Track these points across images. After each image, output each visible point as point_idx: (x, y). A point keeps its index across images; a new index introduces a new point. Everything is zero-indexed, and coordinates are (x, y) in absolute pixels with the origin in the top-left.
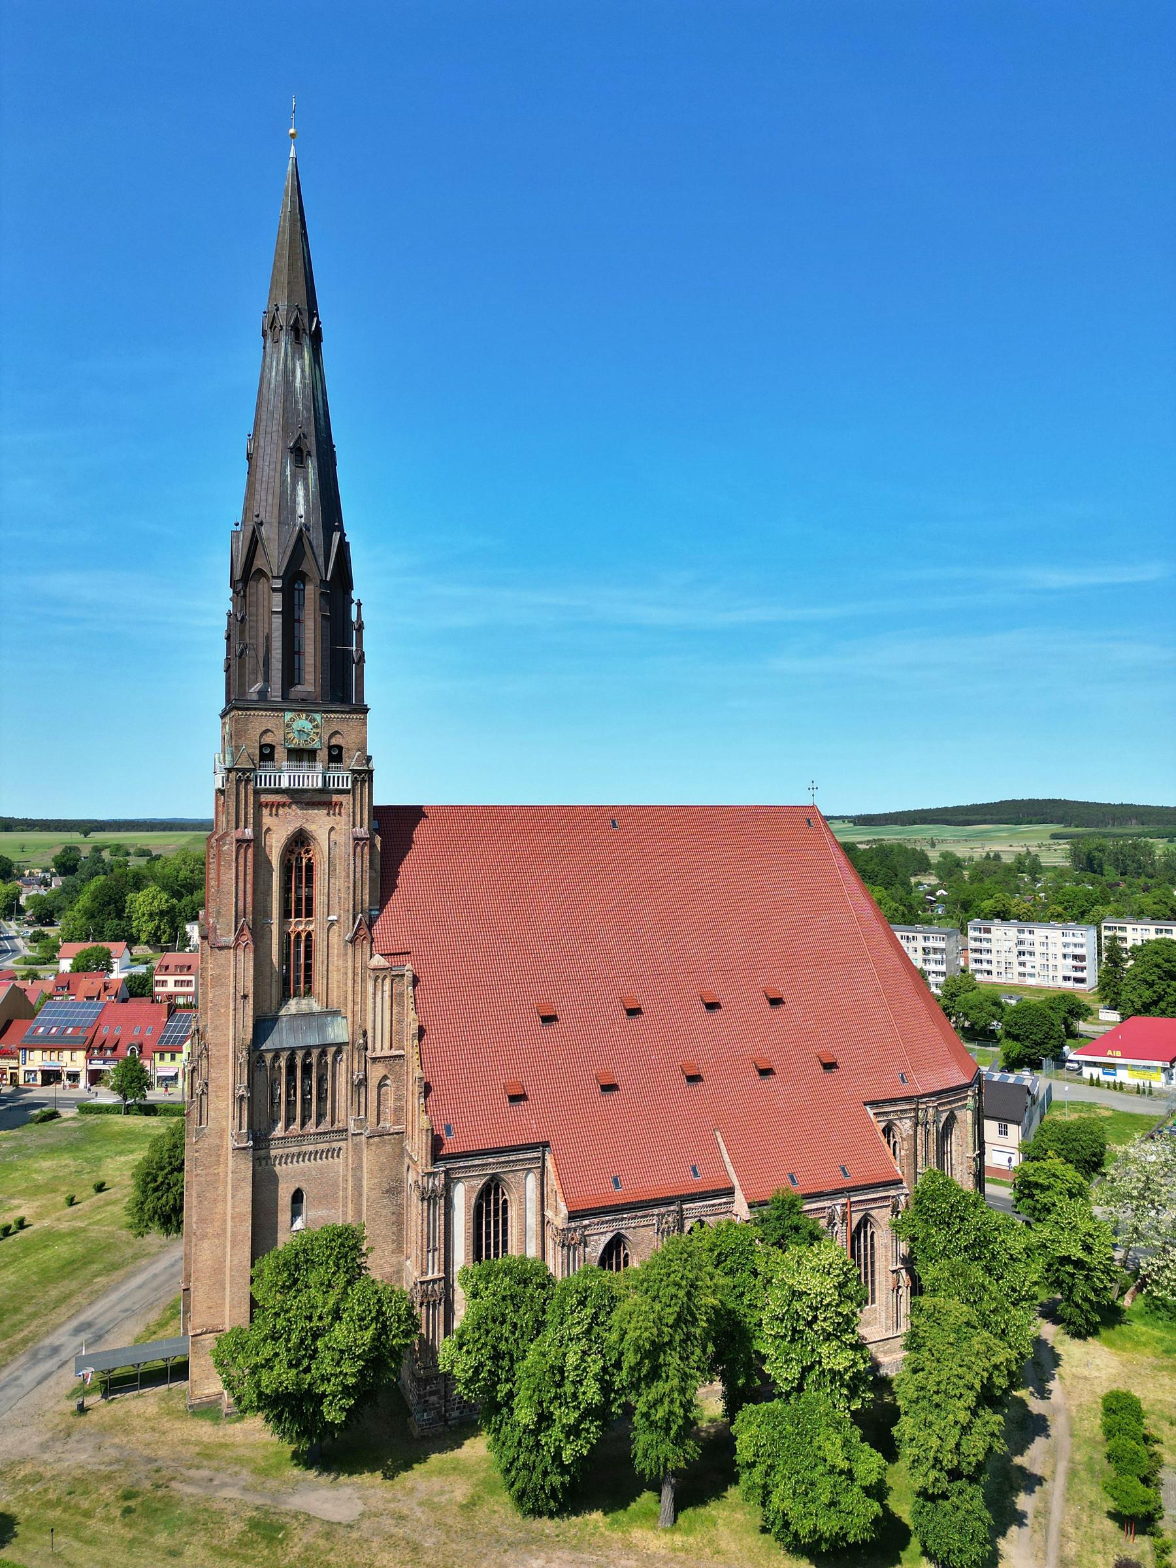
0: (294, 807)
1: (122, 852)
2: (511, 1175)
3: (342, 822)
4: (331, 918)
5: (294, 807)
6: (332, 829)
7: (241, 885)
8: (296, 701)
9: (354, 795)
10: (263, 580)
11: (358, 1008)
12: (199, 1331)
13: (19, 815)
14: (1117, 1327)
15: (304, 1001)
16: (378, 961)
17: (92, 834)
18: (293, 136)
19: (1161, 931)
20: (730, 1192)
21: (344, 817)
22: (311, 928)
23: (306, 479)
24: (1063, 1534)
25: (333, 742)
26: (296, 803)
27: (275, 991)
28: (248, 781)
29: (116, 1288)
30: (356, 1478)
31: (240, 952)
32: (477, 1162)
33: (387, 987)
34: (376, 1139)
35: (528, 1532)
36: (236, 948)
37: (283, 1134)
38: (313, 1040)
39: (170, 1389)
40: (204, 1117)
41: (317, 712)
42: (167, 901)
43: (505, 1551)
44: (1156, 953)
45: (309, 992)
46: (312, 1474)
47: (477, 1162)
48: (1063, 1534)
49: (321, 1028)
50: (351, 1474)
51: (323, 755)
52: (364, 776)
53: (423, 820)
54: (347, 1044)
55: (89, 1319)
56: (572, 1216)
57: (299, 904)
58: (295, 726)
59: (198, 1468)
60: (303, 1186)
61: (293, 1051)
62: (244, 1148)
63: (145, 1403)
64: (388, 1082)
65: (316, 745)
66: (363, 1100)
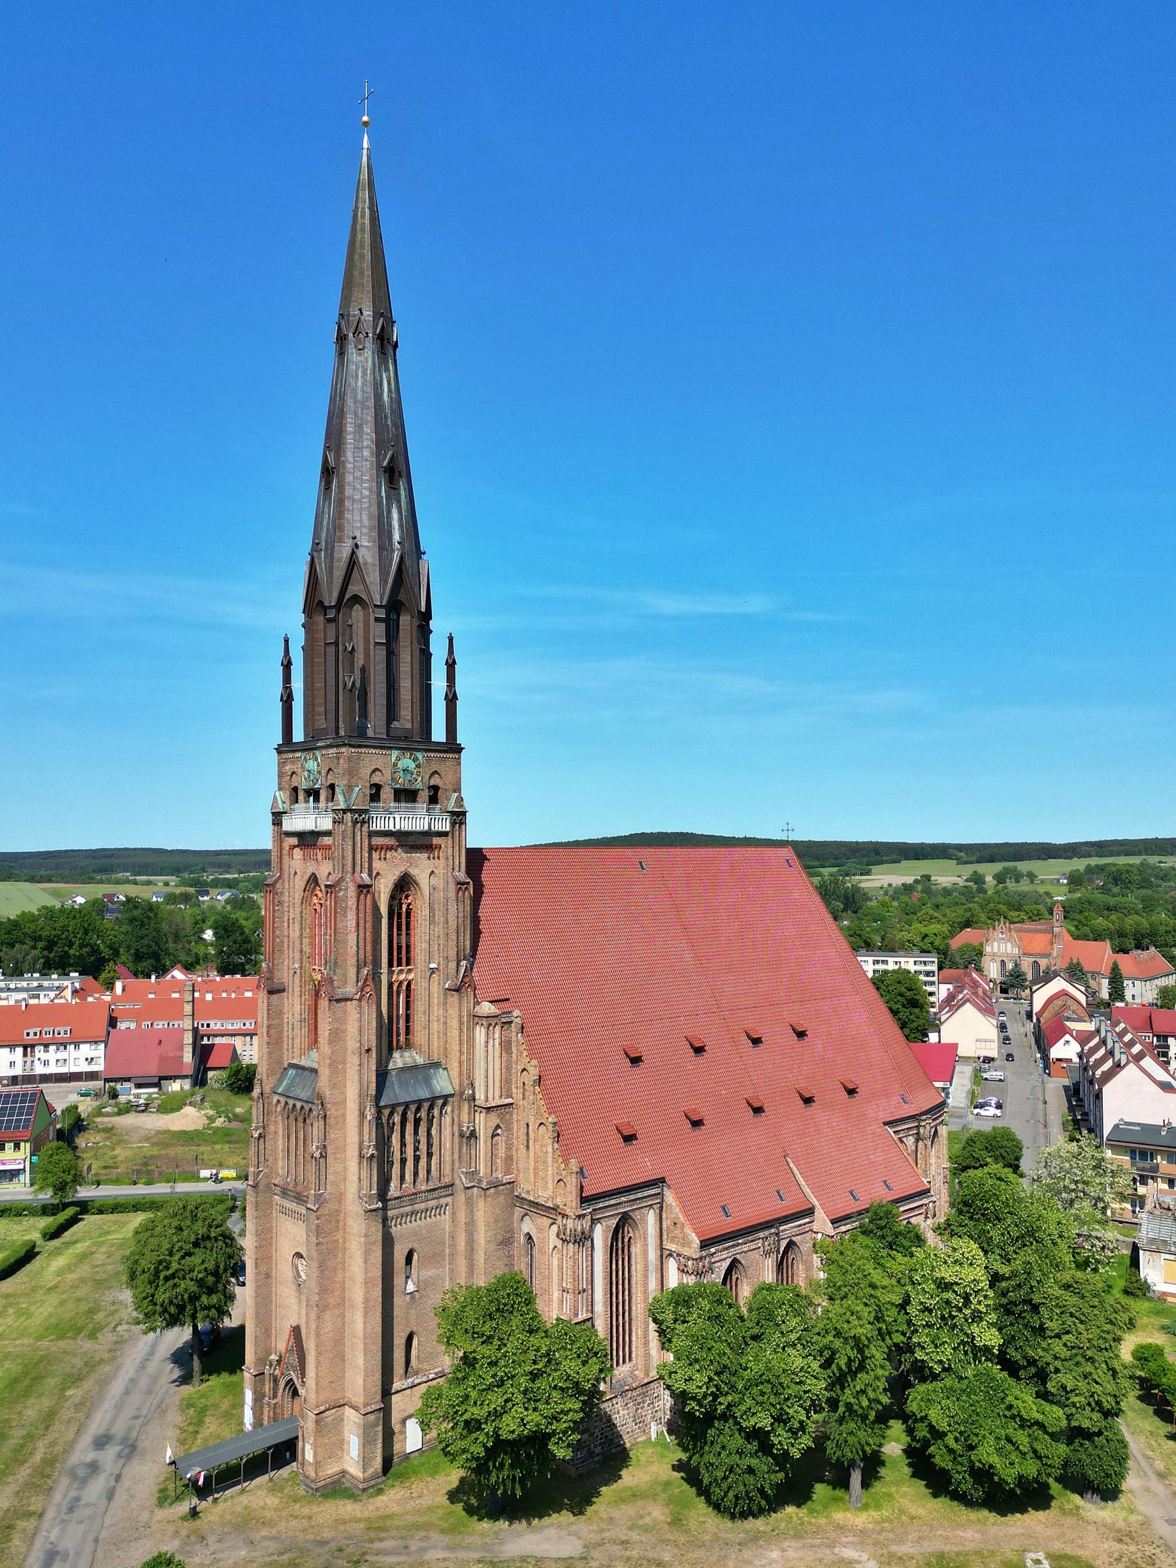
0: (399, 850)
2: (637, 1212)
3: (440, 866)
4: (433, 965)
5: (399, 850)
6: (433, 872)
7: (361, 932)
8: (399, 739)
10: (357, 607)
11: (464, 1057)
12: (322, 1408)
15: (407, 1054)
16: (486, 1008)
18: (366, 124)
19: (878, 962)
20: (810, 1212)
21: (442, 861)
22: (411, 977)
23: (399, 502)
24: (1147, 1458)
25: (432, 783)
26: (402, 846)
28: (363, 822)
29: (101, 1396)
30: (546, 1521)
31: (364, 1003)
32: (613, 1202)
33: (497, 1035)
34: (492, 1190)
35: (747, 1532)
36: (360, 1000)
37: (398, 1194)
38: (424, 1094)
39: (271, 1480)
40: (323, 1182)
41: (419, 750)
43: (740, 1551)
44: (899, 982)
45: (409, 1045)
46: (503, 1524)
47: (613, 1202)
48: (1147, 1458)
49: (427, 1081)
50: (540, 1517)
51: (424, 795)
52: (459, 817)
53: (486, 864)
54: (452, 1095)
55: (101, 1431)
56: (705, 1244)
57: (401, 955)
58: (400, 765)
59: (381, 1540)
60: (416, 1246)
61: (407, 1105)
62: (374, 1210)
63: (256, 1495)
64: (499, 1131)
66: (473, 1152)
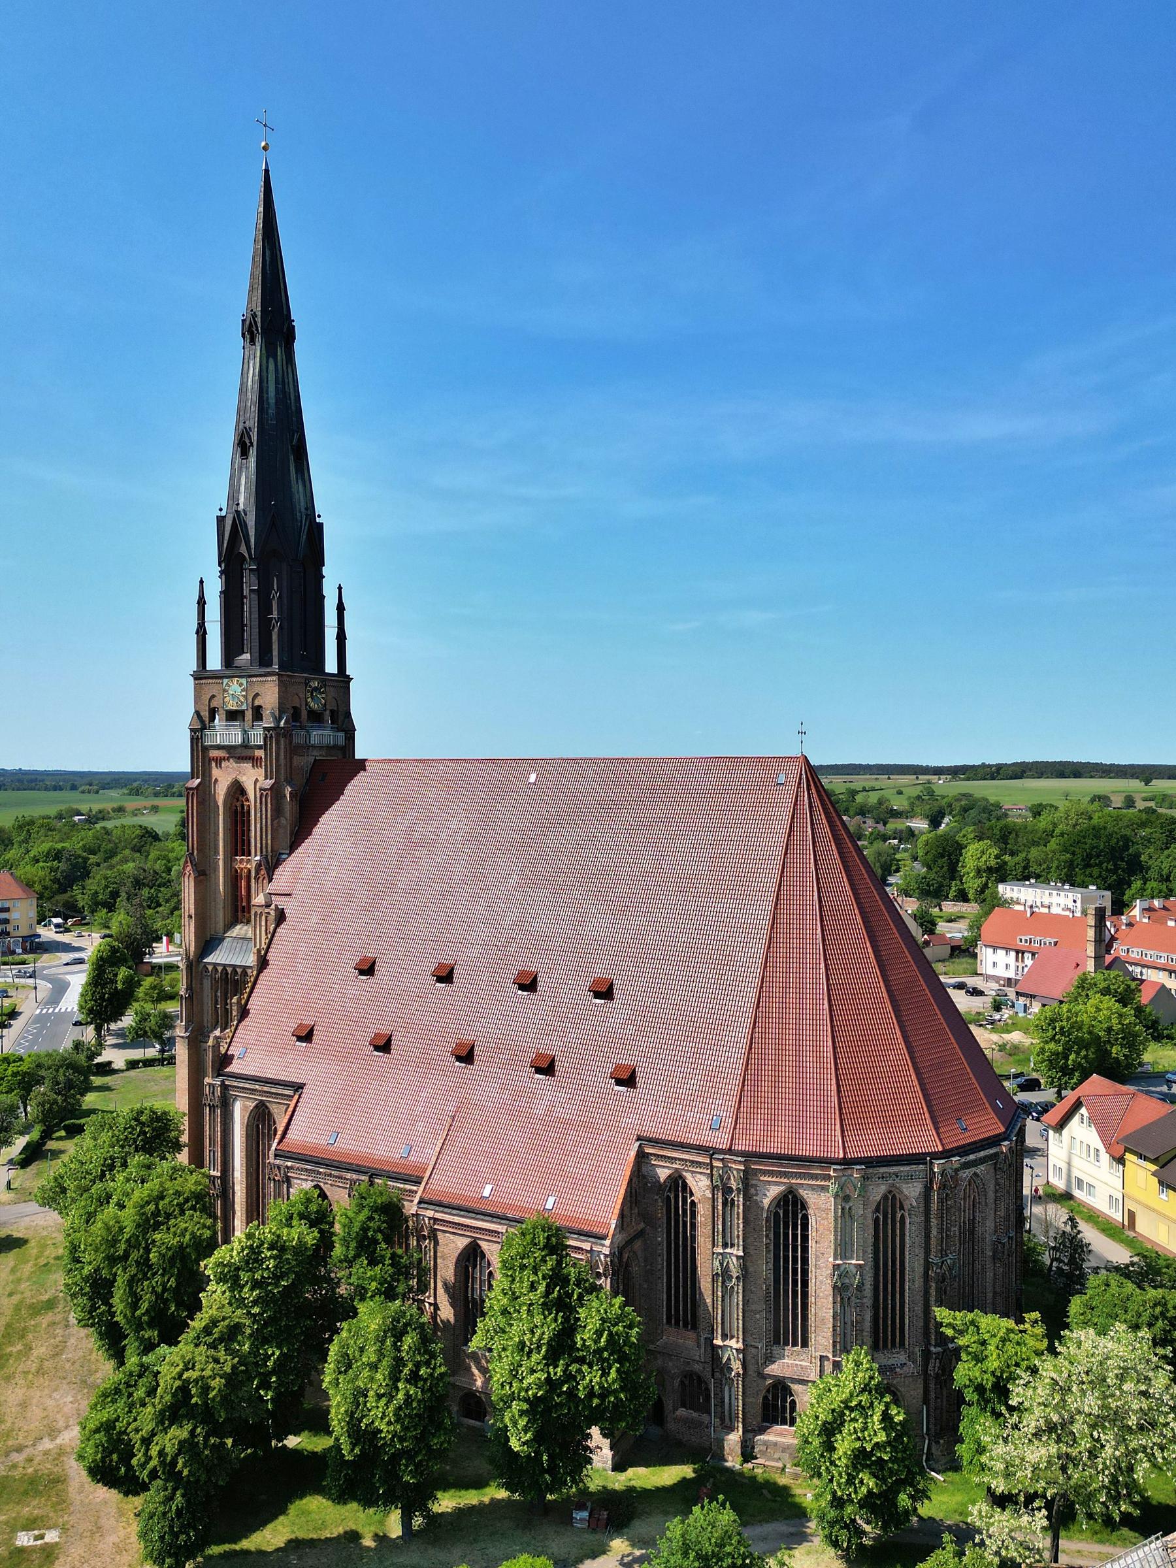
1: (1166, 804)
2: (274, 1106)
9: (265, 750)
13: (1107, 761)
14: (805, 1544)
17: (1154, 782)
27: (220, 915)
42: (997, 857)
53: (362, 773)
65: (244, 707)
